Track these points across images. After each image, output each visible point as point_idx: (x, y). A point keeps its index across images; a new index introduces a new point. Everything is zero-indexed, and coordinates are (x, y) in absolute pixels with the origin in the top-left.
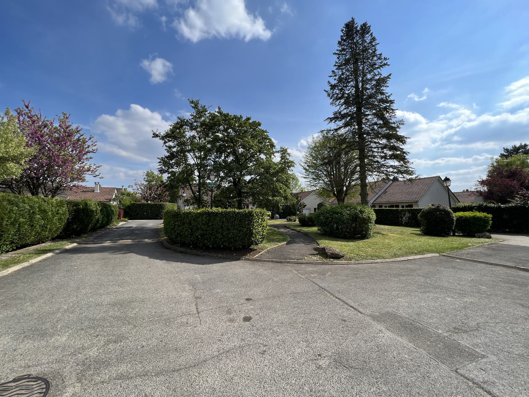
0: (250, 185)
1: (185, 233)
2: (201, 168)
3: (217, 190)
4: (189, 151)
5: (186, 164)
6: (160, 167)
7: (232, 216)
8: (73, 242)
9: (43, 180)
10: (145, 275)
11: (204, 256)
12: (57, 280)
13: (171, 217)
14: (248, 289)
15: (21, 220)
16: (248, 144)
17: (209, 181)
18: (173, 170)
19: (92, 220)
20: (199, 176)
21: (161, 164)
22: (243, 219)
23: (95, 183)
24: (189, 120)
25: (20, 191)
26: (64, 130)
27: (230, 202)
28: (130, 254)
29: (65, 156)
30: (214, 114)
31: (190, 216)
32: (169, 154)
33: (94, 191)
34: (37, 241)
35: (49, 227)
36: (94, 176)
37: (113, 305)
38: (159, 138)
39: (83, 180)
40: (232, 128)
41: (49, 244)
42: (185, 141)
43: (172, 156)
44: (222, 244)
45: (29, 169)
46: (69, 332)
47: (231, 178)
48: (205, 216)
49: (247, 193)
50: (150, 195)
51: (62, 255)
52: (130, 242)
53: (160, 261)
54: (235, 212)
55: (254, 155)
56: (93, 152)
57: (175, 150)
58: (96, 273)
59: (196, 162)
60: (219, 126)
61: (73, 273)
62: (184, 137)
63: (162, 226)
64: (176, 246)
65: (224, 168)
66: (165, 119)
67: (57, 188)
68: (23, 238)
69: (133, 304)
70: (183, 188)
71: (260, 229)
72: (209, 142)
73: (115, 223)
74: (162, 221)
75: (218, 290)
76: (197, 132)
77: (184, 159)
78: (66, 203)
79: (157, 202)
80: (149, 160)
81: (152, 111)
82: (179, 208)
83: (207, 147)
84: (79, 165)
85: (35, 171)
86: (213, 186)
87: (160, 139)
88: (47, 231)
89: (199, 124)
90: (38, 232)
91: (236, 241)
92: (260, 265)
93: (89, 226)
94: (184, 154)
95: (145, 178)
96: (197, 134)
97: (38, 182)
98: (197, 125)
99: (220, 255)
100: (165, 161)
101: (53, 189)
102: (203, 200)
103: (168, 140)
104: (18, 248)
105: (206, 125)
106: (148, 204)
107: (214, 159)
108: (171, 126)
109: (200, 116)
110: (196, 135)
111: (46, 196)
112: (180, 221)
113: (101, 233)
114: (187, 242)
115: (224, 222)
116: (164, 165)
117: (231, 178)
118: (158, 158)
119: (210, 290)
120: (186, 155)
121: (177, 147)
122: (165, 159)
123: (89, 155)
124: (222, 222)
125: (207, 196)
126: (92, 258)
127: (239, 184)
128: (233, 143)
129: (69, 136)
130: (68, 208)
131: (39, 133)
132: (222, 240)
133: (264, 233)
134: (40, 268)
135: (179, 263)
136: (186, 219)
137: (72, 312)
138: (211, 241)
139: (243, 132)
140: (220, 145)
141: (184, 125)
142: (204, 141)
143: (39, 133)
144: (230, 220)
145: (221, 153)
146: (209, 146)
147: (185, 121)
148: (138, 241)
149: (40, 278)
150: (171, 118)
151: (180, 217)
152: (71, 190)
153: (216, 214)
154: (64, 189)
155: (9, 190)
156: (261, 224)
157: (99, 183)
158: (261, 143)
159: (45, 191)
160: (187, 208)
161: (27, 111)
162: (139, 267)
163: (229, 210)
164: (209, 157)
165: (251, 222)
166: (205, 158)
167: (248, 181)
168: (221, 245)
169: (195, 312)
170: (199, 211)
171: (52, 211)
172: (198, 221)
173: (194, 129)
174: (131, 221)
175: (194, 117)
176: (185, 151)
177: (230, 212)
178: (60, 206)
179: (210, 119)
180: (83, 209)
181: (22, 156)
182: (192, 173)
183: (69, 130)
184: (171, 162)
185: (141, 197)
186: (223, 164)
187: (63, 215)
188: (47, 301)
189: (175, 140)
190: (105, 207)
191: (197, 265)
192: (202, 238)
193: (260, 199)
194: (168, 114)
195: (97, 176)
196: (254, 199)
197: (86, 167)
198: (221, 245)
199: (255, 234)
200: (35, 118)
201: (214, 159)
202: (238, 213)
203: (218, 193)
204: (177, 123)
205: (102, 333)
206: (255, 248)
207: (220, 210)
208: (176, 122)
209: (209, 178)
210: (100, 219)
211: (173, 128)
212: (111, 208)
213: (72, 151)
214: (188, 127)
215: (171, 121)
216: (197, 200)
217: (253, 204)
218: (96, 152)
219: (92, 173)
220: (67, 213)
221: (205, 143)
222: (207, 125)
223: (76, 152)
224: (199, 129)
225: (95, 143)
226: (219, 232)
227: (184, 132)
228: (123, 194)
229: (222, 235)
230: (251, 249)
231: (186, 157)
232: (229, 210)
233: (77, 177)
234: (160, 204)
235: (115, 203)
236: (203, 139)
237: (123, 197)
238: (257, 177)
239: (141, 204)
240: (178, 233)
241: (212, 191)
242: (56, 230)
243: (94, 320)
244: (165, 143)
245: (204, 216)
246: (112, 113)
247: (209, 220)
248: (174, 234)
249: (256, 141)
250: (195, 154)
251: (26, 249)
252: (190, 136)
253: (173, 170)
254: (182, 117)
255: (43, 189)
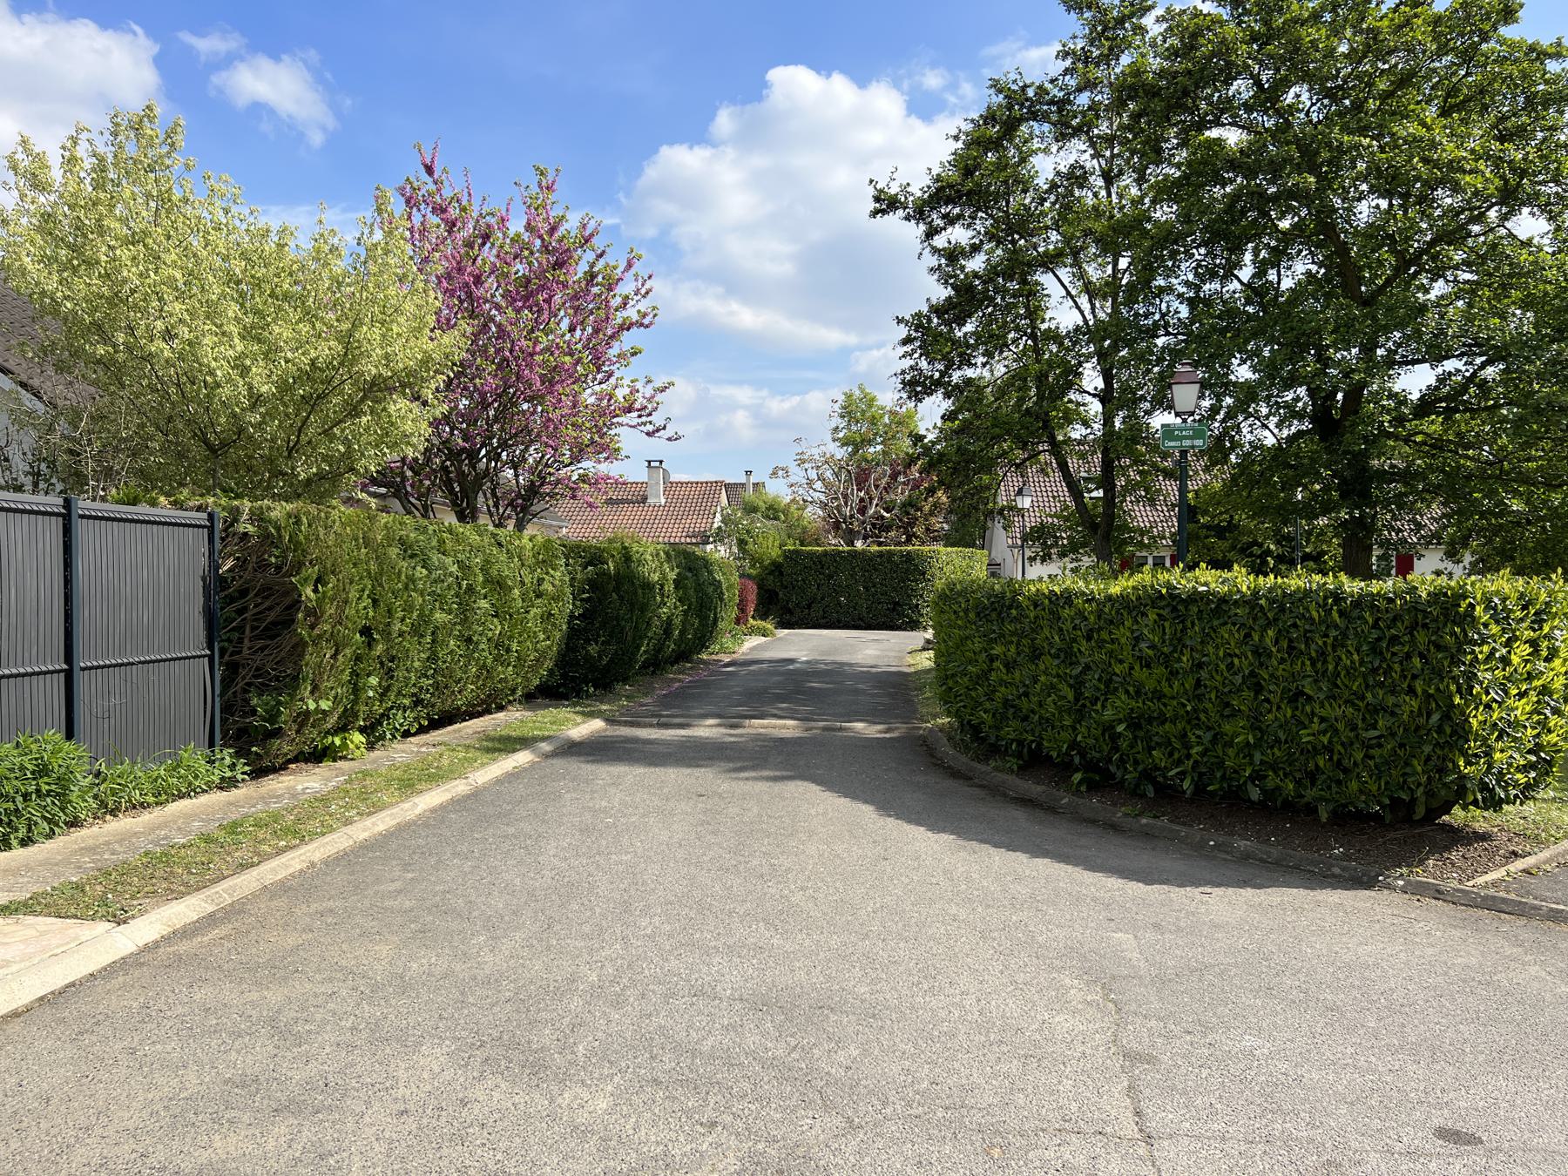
0: (1433, 425)
1: (1040, 705)
2: (1115, 348)
3: (1207, 469)
4: (1049, 262)
5: (1033, 336)
6: (908, 363)
7: (1322, 622)
8: (592, 715)
9: (489, 461)
10: (871, 893)
11: (1147, 835)
12: (555, 861)
13: (972, 615)
14: (1450, 1070)
15: (440, 617)
16: (1425, 161)
17: (1160, 419)
18: (970, 373)
19: (648, 624)
20: (1104, 397)
21: (914, 351)
22: (1394, 640)
23: (649, 462)
24: (1052, 81)
25: (425, 507)
26: (543, 240)
27: (1288, 538)
28: (799, 783)
29: (552, 354)
30: (1197, 14)
31: (1066, 613)
32: (950, 292)
33: (644, 499)
34: (483, 702)
35: (514, 647)
36: (648, 434)
37: (760, 1004)
38: (900, 213)
39: (613, 453)
40: (1307, 77)
41: (518, 714)
42: (1027, 208)
43: (965, 299)
44: (1257, 777)
45: (446, 419)
46: (616, 1079)
47: (1302, 391)
48: (1152, 616)
49: (1406, 476)
50: (862, 510)
51: (559, 763)
52: (794, 728)
53: (930, 834)
54: (1337, 596)
55: (1463, 227)
56: (642, 325)
57: (976, 264)
58: (680, 854)
59: (1089, 317)
60: (1228, 83)
61: (604, 843)
62: (1025, 185)
63: (926, 660)
64: (996, 769)
65: (1255, 335)
66: (923, 107)
67: (532, 491)
68: (446, 687)
69: (833, 1018)
70: (1017, 466)
71: (1522, 708)
72: (1165, 191)
73: (727, 641)
74: (918, 638)
75: (1249, 1041)
76: (1093, 145)
77: (1027, 307)
78: (563, 553)
79: (893, 543)
80: (852, 339)
81: (861, 80)
82: (994, 567)
83: (1149, 219)
84: (597, 388)
85: (464, 425)
86: (1187, 443)
87: (907, 218)
88: (509, 665)
89: (1104, 98)
90: (484, 666)
91: (1346, 771)
92: (1525, 935)
93: (638, 648)
94: (1024, 282)
95: (836, 429)
96: (1093, 157)
97: (474, 468)
98: (1094, 106)
99: (1242, 844)
100: (929, 328)
101: (519, 495)
102: (1125, 527)
103: (945, 216)
104: (435, 725)
105: (1146, 93)
106: (854, 555)
107: (1187, 283)
108: (956, 138)
109: (1111, 49)
110: (1091, 164)
111: (499, 525)
112: (1015, 639)
113: (680, 681)
114: (1054, 754)
115: (1270, 656)
116: (925, 354)
117: (1302, 391)
118: (900, 321)
119: (1207, 1029)
120: (1037, 283)
121: (986, 247)
122: (930, 320)
123: (628, 340)
124: (1256, 653)
125: (1152, 502)
126: (661, 788)
127: (1355, 425)
128: (1313, 169)
129: (559, 265)
130: (570, 573)
131: (469, 270)
132: (1258, 757)
133: (1553, 738)
134: (500, 806)
135: (1022, 857)
136: (1046, 632)
137: (618, 1003)
138: (1188, 756)
139: (1382, 85)
140: (1235, 197)
141: (1021, 120)
142: (1134, 191)
143: (469, 270)
144: (1308, 641)
145: (1237, 248)
146: (1165, 213)
147: (1030, 93)
148: (825, 729)
149: (506, 846)
150: (952, 99)
151: (1016, 620)
152: (574, 497)
153: (1218, 607)
154: (552, 496)
155: (396, 504)
156: (1530, 677)
157: (661, 462)
158: (1521, 134)
159: (496, 506)
160: (1037, 571)
161: (432, 187)
162: (839, 848)
163: (1297, 581)
164: (1160, 282)
165: (1456, 662)
166: (1142, 287)
167: (1415, 396)
168: (1250, 786)
169: (1130, 1130)
170: (1115, 589)
171: (523, 583)
172: (1113, 641)
173: (1077, 132)
174: (786, 631)
175: (1077, 59)
176: (1032, 265)
177: (1307, 593)
178: (544, 561)
179: (1173, 53)
180: (618, 573)
181: (428, 371)
182: (1071, 375)
183: (560, 241)
184: (959, 334)
185: (824, 519)
186: (1250, 309)
187: (556, 599)
188: (535, 942)
189: (979, 209)
190: (690, 570)
191: (1114, 882)
192: (1135, 737)
193: (1505, 511)
194: (933, 80)
195: (658, 430)
196: (1460, 512)
197: (620, 393)
198: (1250, 786)
199: (1485, 740)
200: (454, 212)
201: (1187, 283)
202: (1360, 602)
203: (1218, 485)
204: (990, 117)
205: (728, 1119)
206: (1481, 826)
207: (1241, 579)
208: (983, 111)
209: (1163, 401)
210: (677, 621)
211: (968, 145)
212: (710, 573)
213: (572, 329)
214: (1046, 127)
215: (953, 114)
216: (1093, 527)
217: (1452, 543)
218: (651, 323)
219: (640, 420)
220: (568, 590)
221: (1137, 202)
222: (1152, 92)
223: (583, 330)
224: (1103, 128)
225: (647, 286)
226: (1235, 713)
227: (1023, 160)
228: (751, 509)
229: (1256, 725)
230: (1444, 826)
231: (1032, 293)
232: (1297, 581)
233: (593, 442)
234: (909, 553)
235: (722, 548)
236: (1127, 180)
237: (753, 522)
238: (1483, 366)
239: (825, 553)
240: (1006, 703)
241: (1180, 473)
242: (538, 661)
243: (694, 1057)
244: (931, 233)
245: (1144, 614)
246: (698, 135)
247: (1179, 642)
248: (988, 705)
249: (1477, 134)
250: (1082, 275)
251: (455, 731)
252: (1058, 173)
253: (970, 373)
254: (1012, 76)
255: (489, 495)
